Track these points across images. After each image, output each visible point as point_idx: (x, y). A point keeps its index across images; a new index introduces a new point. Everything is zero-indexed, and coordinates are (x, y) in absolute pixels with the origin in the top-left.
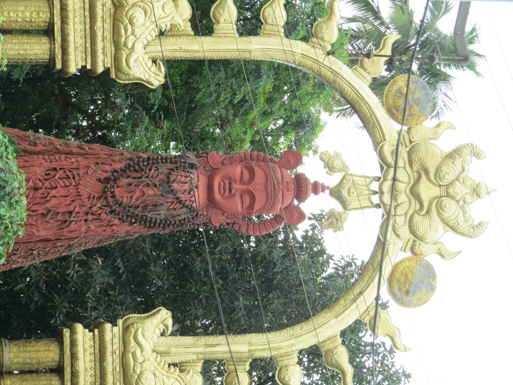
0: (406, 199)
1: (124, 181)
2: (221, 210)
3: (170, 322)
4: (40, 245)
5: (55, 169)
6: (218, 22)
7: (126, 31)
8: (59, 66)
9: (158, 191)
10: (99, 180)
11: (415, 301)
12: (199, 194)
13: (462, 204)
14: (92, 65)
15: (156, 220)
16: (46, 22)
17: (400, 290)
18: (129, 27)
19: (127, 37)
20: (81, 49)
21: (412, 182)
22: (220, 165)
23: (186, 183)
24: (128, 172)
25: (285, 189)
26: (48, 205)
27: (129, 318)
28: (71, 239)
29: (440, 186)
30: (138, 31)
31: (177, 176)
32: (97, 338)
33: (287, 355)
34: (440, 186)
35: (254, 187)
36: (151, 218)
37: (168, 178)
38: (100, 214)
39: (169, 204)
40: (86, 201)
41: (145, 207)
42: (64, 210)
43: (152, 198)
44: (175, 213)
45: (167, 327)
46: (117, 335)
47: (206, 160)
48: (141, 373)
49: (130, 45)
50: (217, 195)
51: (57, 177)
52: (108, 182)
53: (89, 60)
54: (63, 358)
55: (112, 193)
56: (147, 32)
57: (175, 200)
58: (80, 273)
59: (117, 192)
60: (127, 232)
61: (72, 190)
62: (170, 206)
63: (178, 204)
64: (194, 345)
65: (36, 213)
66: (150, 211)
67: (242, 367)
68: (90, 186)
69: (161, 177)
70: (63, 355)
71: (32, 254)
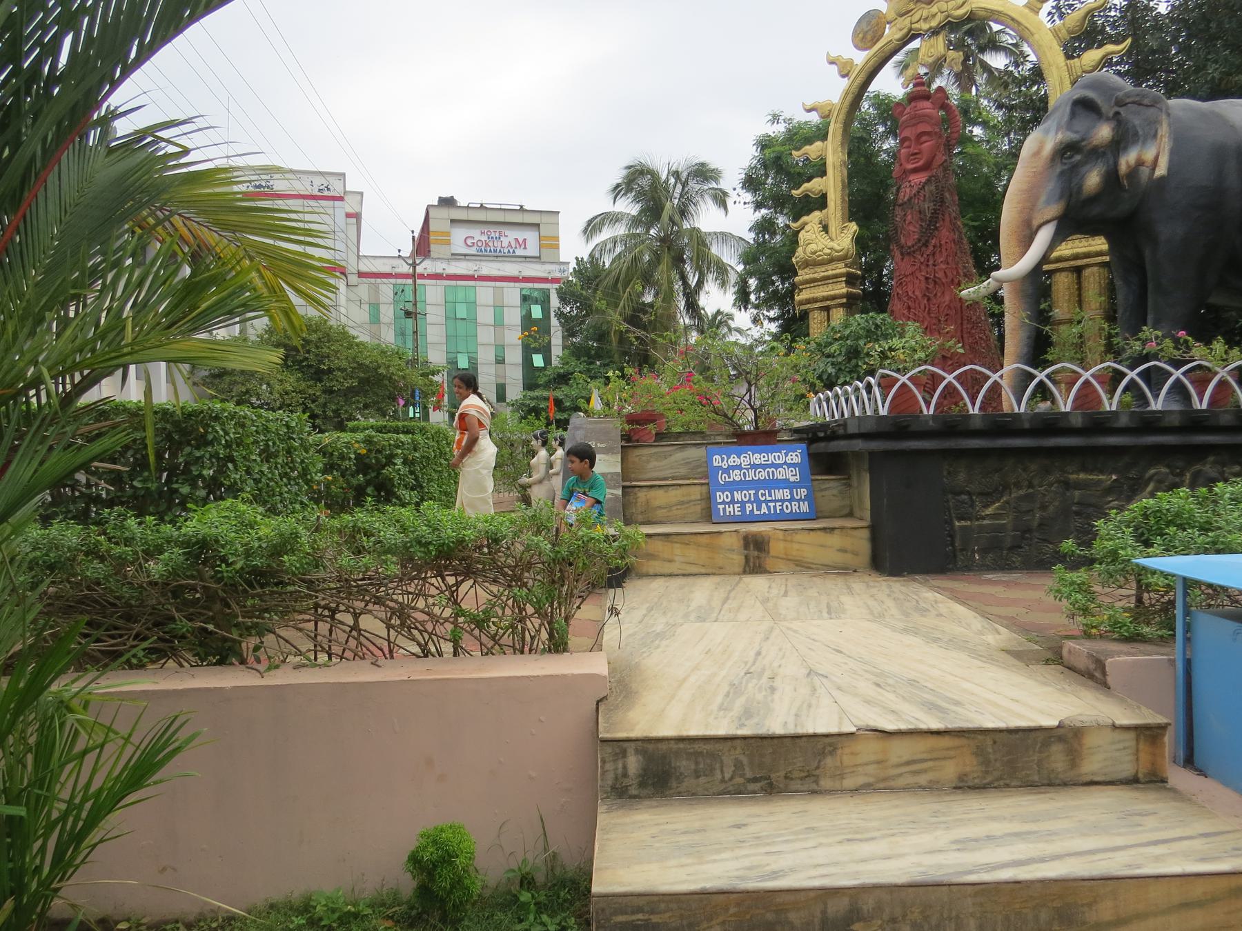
1: (903, 241)
8: (844, 300)
20: (834, 286)
59: (909, 244)
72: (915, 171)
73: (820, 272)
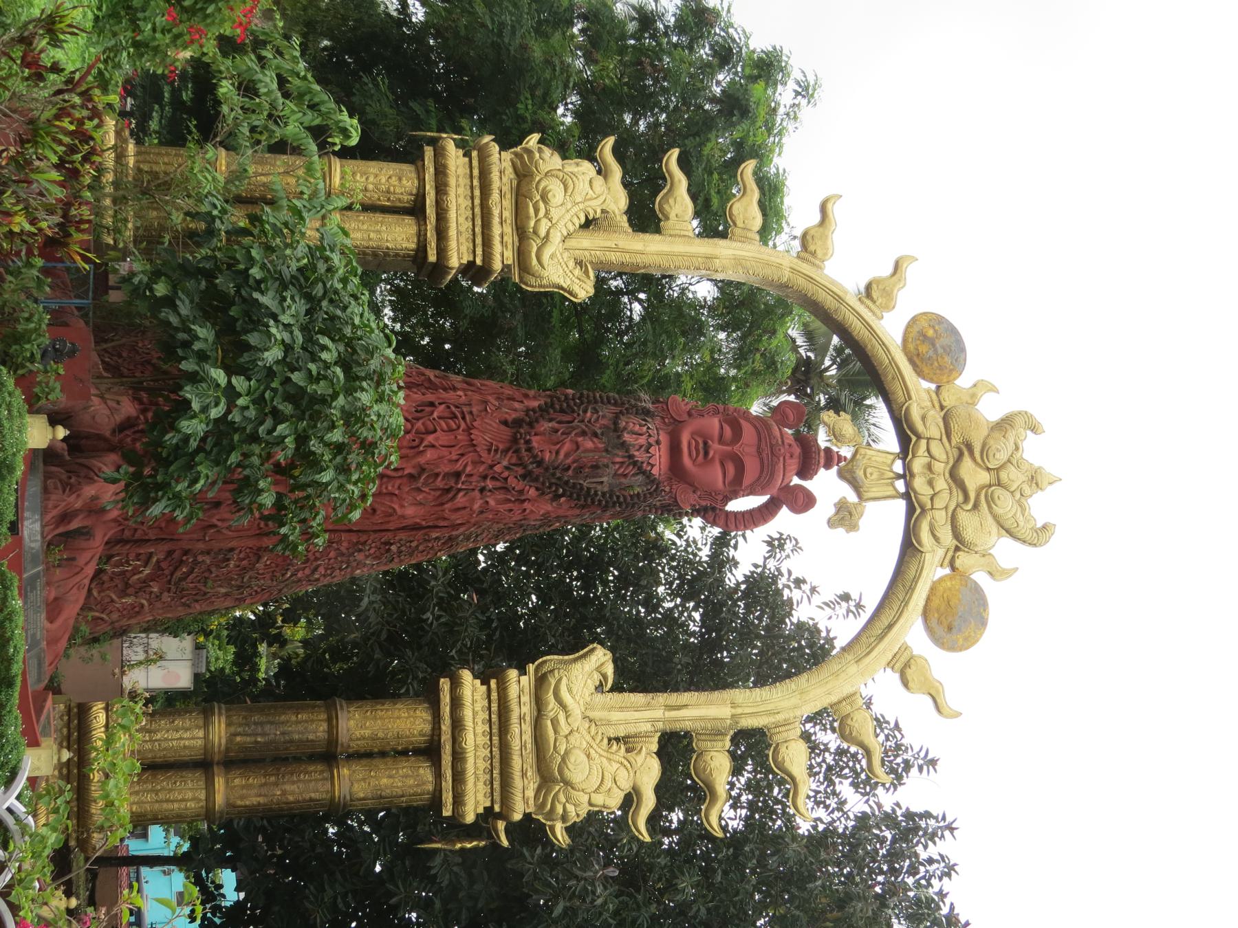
0: (946, 486)
1: (545, 426)
3: (609, 670)
4: (402, 536)
5: (432, 404)
6: (667, 218)
7: (537, 211)
8: (432, 258)
10: (505, 423)
11: (961, 642)
13: (1021, 499)
14: (483, 261)
15: (596, 492)
16: (411, 194)
17: (940, 622)
18: (542, 205)
19: (538, 221)
21: (951, 462)
22: (685, 417)
24: (551, 411)
26: (421, 460)
27: (545, 662)
28: (455, 527)
29: (988, 469)
30: (555, 213)
32: (494, 695)
33: (786, 723)
34: (988, 469)
37: (616, 423)
38: (506, 479)
40: (484, 454)
41: (579, 470)
42: (447, 470)
45: (605, 676)
46: (527, 690)
48: (567, 753)
49: (542, 233)
50: (687, 461)
51: (435, 415)
52: (519, 427)
53: (479, 251)
54: (440, 728)
55: (528, 442)
56: (568, 217)
58: (443, 620)
59: (536, 442)
60: (546, 515)
61: (461, 436)
64: (648, 706)
65: (400, 474)
67: (720, 744)
68: (489, 431)
69: (602, 422)
70: (439, 723)
71: (389, 550)
72: (675, 449)
73: (501, 207)
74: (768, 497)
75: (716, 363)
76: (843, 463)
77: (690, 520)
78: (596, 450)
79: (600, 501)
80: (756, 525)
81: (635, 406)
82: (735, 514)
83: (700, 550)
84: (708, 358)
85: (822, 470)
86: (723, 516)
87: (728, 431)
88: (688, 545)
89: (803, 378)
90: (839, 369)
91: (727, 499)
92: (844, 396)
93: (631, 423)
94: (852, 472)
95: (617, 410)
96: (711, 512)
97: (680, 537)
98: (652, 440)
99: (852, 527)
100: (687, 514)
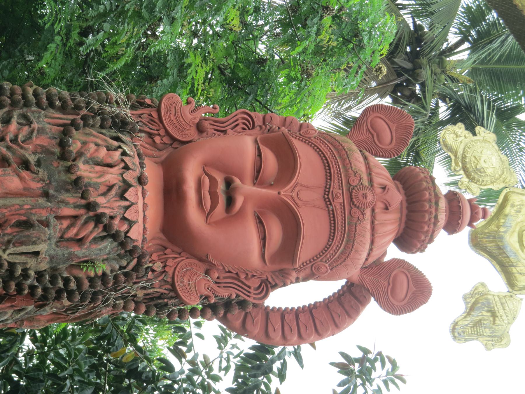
2: (201, 260)
9: (33, 179)
12: (144, 204)
15: (25, 271)
22: (192, 134)
23: (110, 166)
25: (380, 206)
31: (84, 143)
35: (294, 195)
36: (12, 265)
37: (63, 144)
39: (66, 223)
43: (17, 201)
44: (80, 252)
47: (155, 115)
50: (194, 215)
57: (82, 211)
62: (68, 228)
63: (91, 225)
66: (9, 242)
69: (39, 141)
74: (343, 282)
75: (250, 33)
76: (480, 223)
77: (198, 325)
78: (25, 193)
79: (32, 288)
80: (320, 335)
81: (100, 112)
82: (283, 313)
83: (216, 379)
84: (236, 23)
85: (442, 235)
86: (260, 319)
87: (270, 161)
88: (195, 371)
89: (408, 65)
90: (474, 49)
91: (267, 286)
92: (483, 99)
93: (91, 143)
94: (496, 237)
95: (67, 119)
96: (233, 308)
97: (179, 355)
98: (130, 177)
99: (498, 339)
100: (193, 312)
